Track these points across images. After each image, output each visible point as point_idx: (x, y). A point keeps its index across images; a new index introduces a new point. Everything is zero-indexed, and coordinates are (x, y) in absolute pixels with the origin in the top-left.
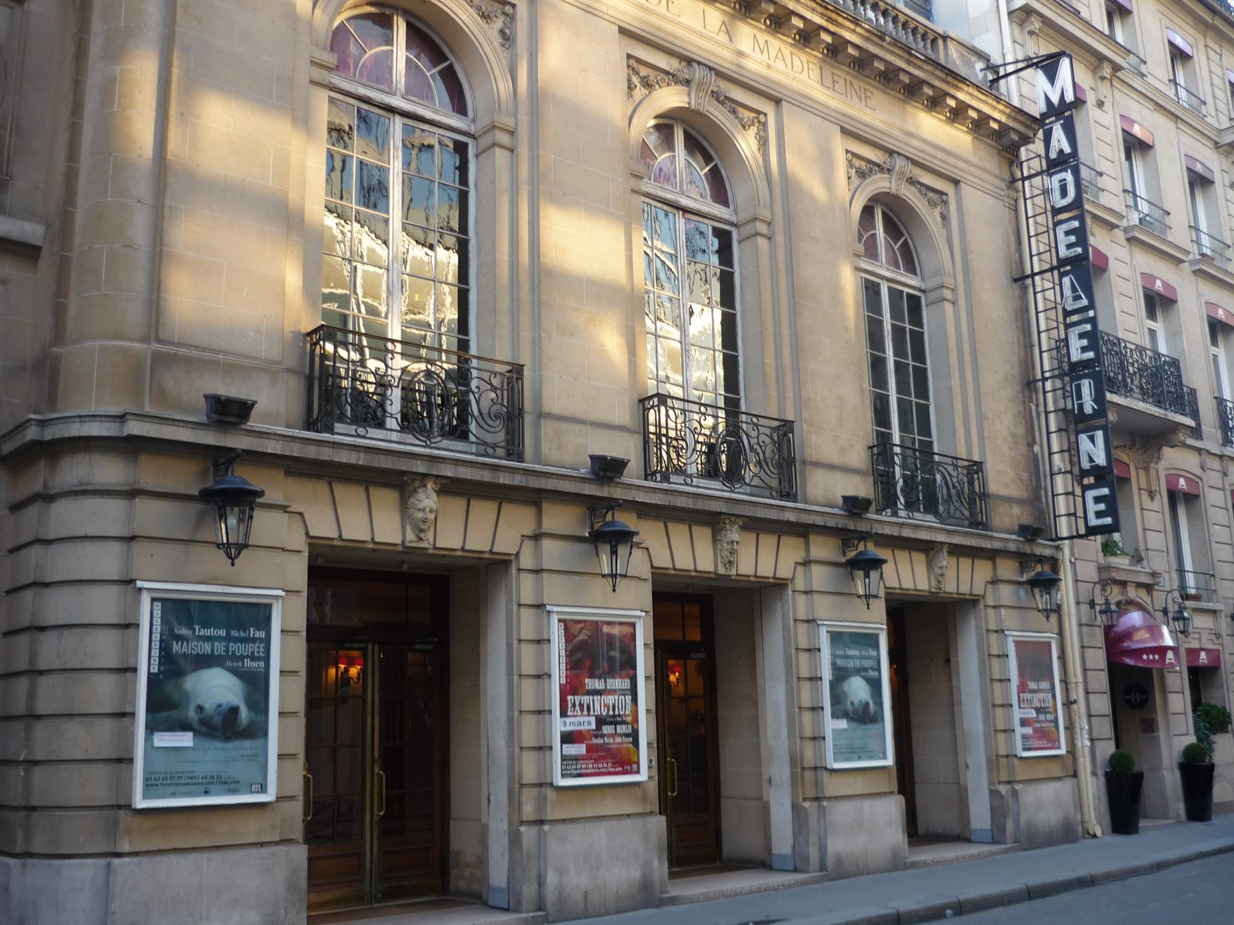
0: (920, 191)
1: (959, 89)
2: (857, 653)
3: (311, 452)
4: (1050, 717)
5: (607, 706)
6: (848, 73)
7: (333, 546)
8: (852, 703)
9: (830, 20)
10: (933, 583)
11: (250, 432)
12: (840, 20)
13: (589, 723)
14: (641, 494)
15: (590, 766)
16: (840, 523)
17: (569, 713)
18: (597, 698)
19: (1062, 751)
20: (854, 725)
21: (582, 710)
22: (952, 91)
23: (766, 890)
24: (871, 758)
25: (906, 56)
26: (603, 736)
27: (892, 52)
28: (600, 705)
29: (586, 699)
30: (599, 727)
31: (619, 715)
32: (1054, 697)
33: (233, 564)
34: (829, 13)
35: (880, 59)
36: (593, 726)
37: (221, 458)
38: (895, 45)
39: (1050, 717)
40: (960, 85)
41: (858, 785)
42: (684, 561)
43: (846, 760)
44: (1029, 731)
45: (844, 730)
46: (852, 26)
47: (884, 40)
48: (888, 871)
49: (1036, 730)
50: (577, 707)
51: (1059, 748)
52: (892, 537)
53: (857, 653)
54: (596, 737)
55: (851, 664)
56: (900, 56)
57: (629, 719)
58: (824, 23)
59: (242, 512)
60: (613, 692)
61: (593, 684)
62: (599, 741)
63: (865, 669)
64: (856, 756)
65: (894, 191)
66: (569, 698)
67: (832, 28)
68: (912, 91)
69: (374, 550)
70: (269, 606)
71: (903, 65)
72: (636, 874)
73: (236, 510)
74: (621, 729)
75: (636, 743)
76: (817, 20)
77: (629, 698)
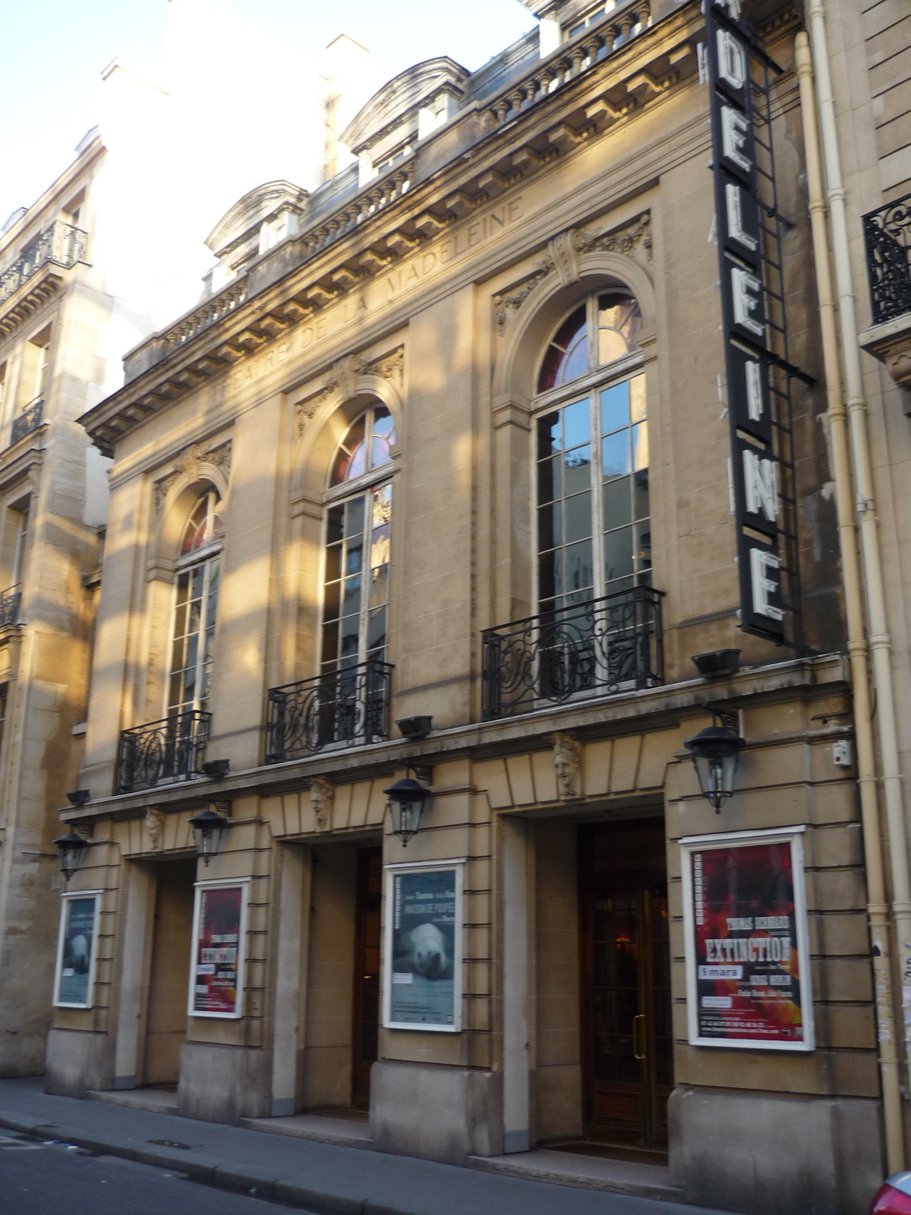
0: (606, 248)
1: (590, 88)
2: (430, 896)
3: (128, 805)
4: (230, 975)
5: (756, 950)
6: (484, 211)
7: (611, 801)
8: (420, 955)
9: (410, 208)
10: (562, 789)
11: (91, 806)
12: (417, 197)
13: (735, 973)
14: (618, 710)
15: (736, 1025)
16: (405, 752)
17: (709, 960)
18: (742, 941)
19: (806, 1045)
20: (420, 981)
21: (725, 956)
22: (583, 101)
23: (314, 1140)
24: (438, 1021)
25: (501, 141)
26: (750, 988)
27: (486, 157)
28: (746, 950)
29: (728, 943)
30: (746, 978)
31: (774, 963)
32: (794, 944)
33: (405, 846)
34: (404, 205)
35: (179, 373)
36: (739, 976)
37: (727, 709)
38: (479, 151)
39: (787, 980)
40: (586, 84)
41: (422, 1051)
42: (523, 797)
43: (407, 1020)
44: (204, 989)
45: (409, 985)
46: (431, 188)
47: (467, 160)
48: (442, 1161)
49: (212, 989)
50: (719, 953)
51: (800, 1039)
52: (469, 749)
53: (430, 896)
54: (744, 988)
55: (421, 909)
56: (394, 218)
57: (787, 967)
58: (408, 215)
59: (75, 853)
60: (764, 933)
61: (737, 923)
62: (746, 994)
63: (439, 915)
64: (421, 1016)
65: (575, 276)
66: (708, 942)
67: (416, 211)
68: (550, 152)
69: (645, 797)
70: (453, 872)
71: (506, 151)
72: (225, 1094)
73: (72, 851)
74: (775, 980)
75: (797, 999)
76: (402, 220)
77: (786, 941)
